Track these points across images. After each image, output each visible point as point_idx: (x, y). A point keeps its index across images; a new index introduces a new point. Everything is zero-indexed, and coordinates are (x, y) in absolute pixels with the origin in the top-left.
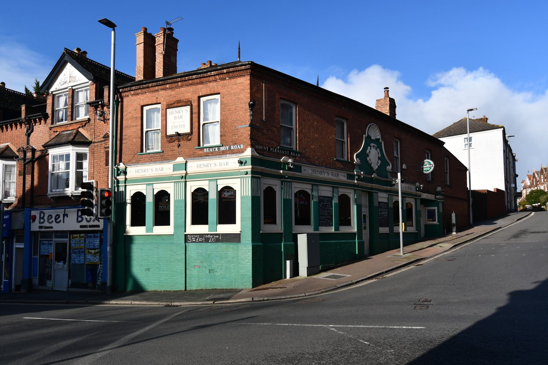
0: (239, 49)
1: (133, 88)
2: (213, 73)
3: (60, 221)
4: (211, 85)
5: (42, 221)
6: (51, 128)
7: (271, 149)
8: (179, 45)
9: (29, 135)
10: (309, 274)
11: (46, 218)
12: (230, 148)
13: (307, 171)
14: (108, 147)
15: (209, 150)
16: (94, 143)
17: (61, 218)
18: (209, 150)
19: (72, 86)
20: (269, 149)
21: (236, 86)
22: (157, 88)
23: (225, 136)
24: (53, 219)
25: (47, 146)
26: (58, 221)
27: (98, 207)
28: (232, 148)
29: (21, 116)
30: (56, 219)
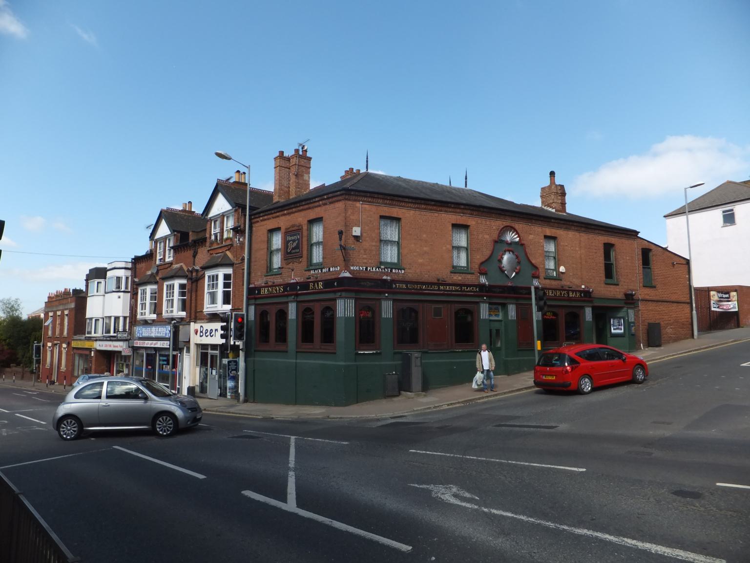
0: (367, 162)
1: (261, 215)
2: (317, 199)
3: (213, 335)
4: (318, 210)
5: (202, 334)
6: (208, 251)
7: (369, 269)
8: (313, 163)
9: (194, 256)
10: (103, 382)
11: (204, 332)
12: (322, 271)
14: (244, 269)
15: (315, 271)
16: (236, 264)
17: (213, 333)
18: (315, 271)
19: (223, 213)
20: (366, 269)
21: (334, 210)
22: (278, 214)
23: (326, 258)
24: (208, 333)
25: (206, 268)
26: (211, 335)
27: (460, 291)
28: (331, 270)
29: (189, 240)
30: (210, 333)
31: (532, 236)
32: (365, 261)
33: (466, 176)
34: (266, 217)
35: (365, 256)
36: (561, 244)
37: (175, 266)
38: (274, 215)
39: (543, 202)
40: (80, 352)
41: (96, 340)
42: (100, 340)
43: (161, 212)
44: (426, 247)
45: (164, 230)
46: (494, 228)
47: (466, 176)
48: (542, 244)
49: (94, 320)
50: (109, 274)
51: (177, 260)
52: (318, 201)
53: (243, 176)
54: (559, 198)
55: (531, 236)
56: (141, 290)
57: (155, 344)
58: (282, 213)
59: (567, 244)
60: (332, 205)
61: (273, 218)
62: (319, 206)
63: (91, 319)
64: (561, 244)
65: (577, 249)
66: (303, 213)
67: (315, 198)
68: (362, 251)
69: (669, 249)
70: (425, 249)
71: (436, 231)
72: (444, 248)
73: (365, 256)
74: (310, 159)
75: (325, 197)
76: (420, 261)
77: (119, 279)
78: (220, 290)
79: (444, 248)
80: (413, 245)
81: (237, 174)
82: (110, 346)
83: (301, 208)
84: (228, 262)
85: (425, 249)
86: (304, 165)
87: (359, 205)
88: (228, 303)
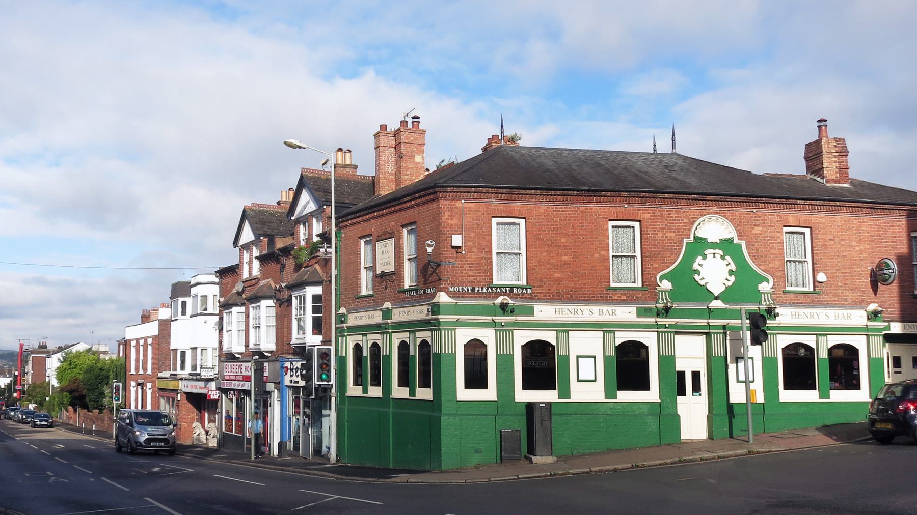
4: (410, 212)
7: (477, 289)
13: (544, 311)
31: (760, 228)
32: (472, 279)
33: (673, 135)
34: (355, 220)
35: (470, 273)
36: (820, 237)
37: (262, 283)
38: (364, 218)
39: (808, 168)
40: (166, 394)
41: (181, 379)
42: (186, 379)
43: (244, 210)
44: (566, 255)
45: (248, 235)
46: (685, 221)
47: (673, 135)
48: (779, 240)
49: (199, 351)
50: (193, 291)
51: (265, 274)
52: (410, 201)
53: (348, 155)
54: (835, 159)
55: (756, 228)
56: (296, 297)
57: (243, 385)
58: (370, 216)
59: (831, 237)
60: (426, 206)
61: (364, 221)
62: (412, 207)
63: (175, 350)
64: (820, 237)
65: (854, 243)
66: (395, 216)
67: (403, 197)
68: (466, 267)
69: (708, 287)
70: (564, 258)
71: (581, 232)
72: (596, 255)
73: (470, 273)
74: (423, 132)
75: (417, 195)
76: (556, 275)
77: (205, 298)
78: (309, 316)
79: (596, 255)
80: (545, 254)
81: (340, 153)
82: (196, 387)
83: (393, 209)
84: (316, 279)
85: (564, 258)
86: (416, 141)
87: (461, 204)
88: (320, 333)
